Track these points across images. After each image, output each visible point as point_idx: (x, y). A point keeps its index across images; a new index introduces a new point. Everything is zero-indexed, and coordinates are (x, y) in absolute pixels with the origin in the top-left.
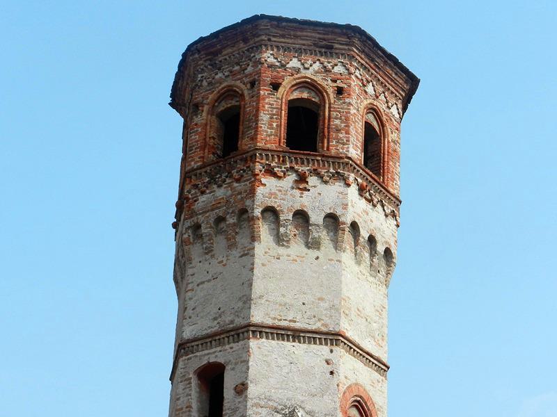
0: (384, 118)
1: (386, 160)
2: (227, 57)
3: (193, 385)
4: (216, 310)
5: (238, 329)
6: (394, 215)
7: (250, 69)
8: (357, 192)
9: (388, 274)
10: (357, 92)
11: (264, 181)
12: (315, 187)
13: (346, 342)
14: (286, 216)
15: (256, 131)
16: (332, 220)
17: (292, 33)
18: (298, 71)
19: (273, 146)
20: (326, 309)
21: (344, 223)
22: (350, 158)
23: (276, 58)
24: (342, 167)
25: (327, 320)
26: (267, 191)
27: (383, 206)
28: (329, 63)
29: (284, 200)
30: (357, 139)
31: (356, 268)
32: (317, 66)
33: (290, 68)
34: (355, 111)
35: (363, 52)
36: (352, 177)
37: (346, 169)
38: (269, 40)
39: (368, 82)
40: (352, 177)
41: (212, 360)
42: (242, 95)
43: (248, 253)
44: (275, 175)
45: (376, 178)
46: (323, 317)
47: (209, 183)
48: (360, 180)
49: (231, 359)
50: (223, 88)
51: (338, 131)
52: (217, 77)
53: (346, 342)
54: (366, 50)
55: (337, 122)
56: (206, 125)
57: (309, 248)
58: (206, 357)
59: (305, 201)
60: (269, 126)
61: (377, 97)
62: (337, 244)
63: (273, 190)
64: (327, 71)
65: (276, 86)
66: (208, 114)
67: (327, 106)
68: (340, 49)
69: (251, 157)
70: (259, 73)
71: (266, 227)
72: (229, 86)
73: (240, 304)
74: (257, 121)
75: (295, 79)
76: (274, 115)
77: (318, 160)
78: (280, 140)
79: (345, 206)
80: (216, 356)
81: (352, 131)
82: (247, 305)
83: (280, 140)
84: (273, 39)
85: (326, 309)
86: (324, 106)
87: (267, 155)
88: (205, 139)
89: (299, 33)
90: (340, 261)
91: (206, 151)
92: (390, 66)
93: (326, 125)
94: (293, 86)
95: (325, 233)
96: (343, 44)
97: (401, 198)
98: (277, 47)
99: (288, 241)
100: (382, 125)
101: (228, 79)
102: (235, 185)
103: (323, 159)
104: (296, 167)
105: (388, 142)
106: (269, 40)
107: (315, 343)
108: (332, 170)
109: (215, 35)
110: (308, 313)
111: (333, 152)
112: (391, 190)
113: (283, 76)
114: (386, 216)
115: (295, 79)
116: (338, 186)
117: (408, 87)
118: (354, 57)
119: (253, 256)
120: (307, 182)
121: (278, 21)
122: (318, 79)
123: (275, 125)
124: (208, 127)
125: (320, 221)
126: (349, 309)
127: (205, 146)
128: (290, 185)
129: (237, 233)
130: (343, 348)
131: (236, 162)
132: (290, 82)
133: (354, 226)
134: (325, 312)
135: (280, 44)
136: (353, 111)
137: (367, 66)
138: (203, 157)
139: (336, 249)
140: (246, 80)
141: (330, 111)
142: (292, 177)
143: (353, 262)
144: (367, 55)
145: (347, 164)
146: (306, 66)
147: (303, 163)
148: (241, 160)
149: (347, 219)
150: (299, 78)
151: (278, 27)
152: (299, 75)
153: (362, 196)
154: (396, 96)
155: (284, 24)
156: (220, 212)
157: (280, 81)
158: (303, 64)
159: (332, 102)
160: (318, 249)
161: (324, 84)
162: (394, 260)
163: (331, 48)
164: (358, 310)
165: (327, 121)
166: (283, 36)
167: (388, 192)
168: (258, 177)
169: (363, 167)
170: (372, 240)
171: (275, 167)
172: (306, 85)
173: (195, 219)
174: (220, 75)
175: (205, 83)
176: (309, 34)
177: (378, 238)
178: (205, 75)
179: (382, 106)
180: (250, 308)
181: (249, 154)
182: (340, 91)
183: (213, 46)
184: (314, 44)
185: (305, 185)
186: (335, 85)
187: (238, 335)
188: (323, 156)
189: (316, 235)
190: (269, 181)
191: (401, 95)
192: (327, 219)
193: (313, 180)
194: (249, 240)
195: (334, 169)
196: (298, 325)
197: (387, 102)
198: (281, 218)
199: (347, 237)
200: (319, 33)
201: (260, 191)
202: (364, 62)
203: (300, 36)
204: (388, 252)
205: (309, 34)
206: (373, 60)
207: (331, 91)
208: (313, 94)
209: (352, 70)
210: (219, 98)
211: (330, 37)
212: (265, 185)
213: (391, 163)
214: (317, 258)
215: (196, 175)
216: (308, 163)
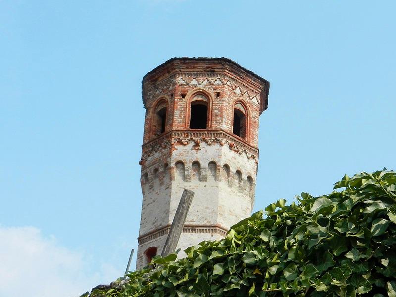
0: (248, 105)
1: (249, 128)
2: (161, 82)
3: (143, 260)
4: (154, 219)
5: (163, 228)
6: (253, 157)
7: (171, 87)
8: (228, 148)
9: (251, 189)
10: (228, 93)
11: (176, 147)
12: (204, 148)
13: (221, 230)
14: (188, 165)
15: (173, 121)
16: (213, 165)
17: (192, 66)
18: (196, 86)
19: (182, 128)
20: (210, 213)
21: (219, 166)
22: (223, 130)
23: (184, 80)
24: (218, 136)
25: (210, 219)
26: (178, 152)
27: (246, 153)
28: (212, 79)
29: (187, 156)
30: (228, 119)
31: (229, 189)
32: (206, 82)
33: (191, 85)
34: (227, 104)
35: (232, 71)
36: (224, 140)
37: (221, 136)
38: (180, 71)
39: (236, 87)
40: (224, 140)
41: (151, 246)
42: (167, 102)
43: (169, 187)
44: (182, 143)
45: (241, 139)
46: (208, 218)
47: (152, 150)
48: (229, 141)
49: (160, 244)
50: (159, 99)
51: (217, 116)
52: (157, 93)
53: (221, 230)
54: (234, 70)
55: (216, 111)
56: (151, 119)
57: (201, 181)
58: (149, 245)
59: (199, 156)
60: (181, 116)
61: (243, 95)
62: (216, 177)
63: (181, 152)
64: (211, 84)
65: (183, 95)
66: (152, 113)
67: (211, 103)
68: (218, 71)
69: (170, 135)
70: (175, 89)
71: (178, 172)
72: (162, 97)
73: (165, 215)
74: (173, 115)
75: (194, 91)
76: (182, 111)
77: (205, 133)
78: (185, 124)
79: (220, 157)
80: (153, 244)
81: (225, 115)
82: (168, 215)
83: (185, 124)
84: (182, 70)
85: (210, 213)
86: (210, 103)
87: (178, 133)
88: (151, 127)
89: (196, 66)
90: (217, 187)
91: (151, 133)
92: (250, 77)
93: (210, 114)
94: (193, 94)
95: (210, 172)
96: (220, 69)
97: (258, 148)
98: (185, 74)
99: (189, 179)
100: (246, 109)
101: (161, 93)
102: (163, 150)
103: (209, 132)
104: (193, 138)
105: (250, 118)
106: (180, 71)
107: (204, 232)
108: (213, 138)
109: (155, 71)
110: (200, 216)
111: (214, 128)
112: (252, 144)
113: (188, 90)
114: (249, 158)
115: (194, 91)
116: (216, 146)
117: (263, 87)
118: (226, 75)
119: (171, 188)
120: (200, 146)
121: (184, 60)
122: (207, 89)
123: (182, 116)
124: (152, 120)
125: (207, 166)
126: (224, 212)
127: (151, 130)
128: (191, 148)
129: (164, 177)
130: (219, 233)
131: (163, 138)
132: (191, 92)
133: (226, 167)
134: (209, 215)
135: (186, 73)
136: (225, 104)
137: (235, 78)
138: (149, 137)
139: (216, 180)
140: (169, 94)
141: (212, 106)
142: (192, 143)
143: (227, 186)
144: (235, 73)
145: (221, 134)
146: (200, 83)
147: (197, 136)
148: (166, 137)
149: (221, 163)
150: (196, 90)
151: (184, 63)
152: (196, 88)
153: (231, 150)
154: (256, 92)
155: (187, 61)
156: (156, 166)
157: (186, 92)
158: (198, 82)
159: (214, 101)
160: (206, 181)
161: (209, 91)
162: (254, 182)
163: (214, 71)
164: (230, 211)
165: (211, 111)
166: (187, 68)
167: (250, 145)
168: (173, 146)
169: (233, 134)
170: (239, 173)
171: (182, 139)
172: (200, 93)
173: (145, 170)
174: (158, 92)
175: (151, 97)
176: (201, 65)
177: (243, 171)
178: (151, 92)
179: (245, 99)
180: (169, 216)
181: (169, 134)
182: (218, 94)
183: (154, 76)
184: (205, 71)
185: (199, 147)
186: (216, 91)
187: (164, 231)
188: (208, 131)
189: (204, 173)
190: (179, 147)
191: (260, 91)
192: (211, 164)
193: (203, 144)
194: (169, 180)
195: (214, 137)
196: (194, 224)
197: (249, 96)
198: (185, 167)
199: (222, 173)
200: (207, 64)
201: (174, 153)
202: (233, 77)
203: (196, 67)
204: (250, 178)
205: (201, 65)
206: (238, 75)
207: (213, 95)
208: (204, 97)
209: (225, 82)
210: (158, 103)
211: (212, 65)
212: (177, 149)
213: (252, 129)
214: (205, 186)
215: (146, 147)
216: (200, 135)
